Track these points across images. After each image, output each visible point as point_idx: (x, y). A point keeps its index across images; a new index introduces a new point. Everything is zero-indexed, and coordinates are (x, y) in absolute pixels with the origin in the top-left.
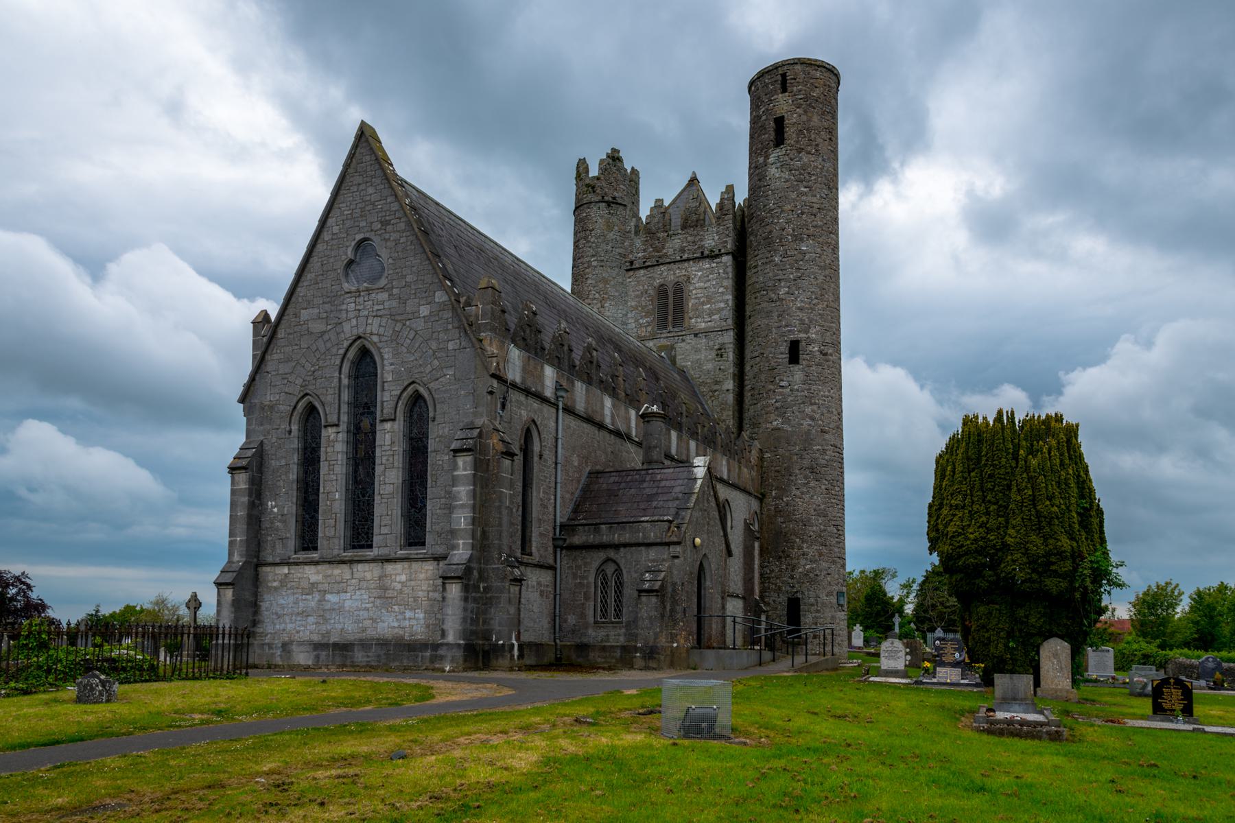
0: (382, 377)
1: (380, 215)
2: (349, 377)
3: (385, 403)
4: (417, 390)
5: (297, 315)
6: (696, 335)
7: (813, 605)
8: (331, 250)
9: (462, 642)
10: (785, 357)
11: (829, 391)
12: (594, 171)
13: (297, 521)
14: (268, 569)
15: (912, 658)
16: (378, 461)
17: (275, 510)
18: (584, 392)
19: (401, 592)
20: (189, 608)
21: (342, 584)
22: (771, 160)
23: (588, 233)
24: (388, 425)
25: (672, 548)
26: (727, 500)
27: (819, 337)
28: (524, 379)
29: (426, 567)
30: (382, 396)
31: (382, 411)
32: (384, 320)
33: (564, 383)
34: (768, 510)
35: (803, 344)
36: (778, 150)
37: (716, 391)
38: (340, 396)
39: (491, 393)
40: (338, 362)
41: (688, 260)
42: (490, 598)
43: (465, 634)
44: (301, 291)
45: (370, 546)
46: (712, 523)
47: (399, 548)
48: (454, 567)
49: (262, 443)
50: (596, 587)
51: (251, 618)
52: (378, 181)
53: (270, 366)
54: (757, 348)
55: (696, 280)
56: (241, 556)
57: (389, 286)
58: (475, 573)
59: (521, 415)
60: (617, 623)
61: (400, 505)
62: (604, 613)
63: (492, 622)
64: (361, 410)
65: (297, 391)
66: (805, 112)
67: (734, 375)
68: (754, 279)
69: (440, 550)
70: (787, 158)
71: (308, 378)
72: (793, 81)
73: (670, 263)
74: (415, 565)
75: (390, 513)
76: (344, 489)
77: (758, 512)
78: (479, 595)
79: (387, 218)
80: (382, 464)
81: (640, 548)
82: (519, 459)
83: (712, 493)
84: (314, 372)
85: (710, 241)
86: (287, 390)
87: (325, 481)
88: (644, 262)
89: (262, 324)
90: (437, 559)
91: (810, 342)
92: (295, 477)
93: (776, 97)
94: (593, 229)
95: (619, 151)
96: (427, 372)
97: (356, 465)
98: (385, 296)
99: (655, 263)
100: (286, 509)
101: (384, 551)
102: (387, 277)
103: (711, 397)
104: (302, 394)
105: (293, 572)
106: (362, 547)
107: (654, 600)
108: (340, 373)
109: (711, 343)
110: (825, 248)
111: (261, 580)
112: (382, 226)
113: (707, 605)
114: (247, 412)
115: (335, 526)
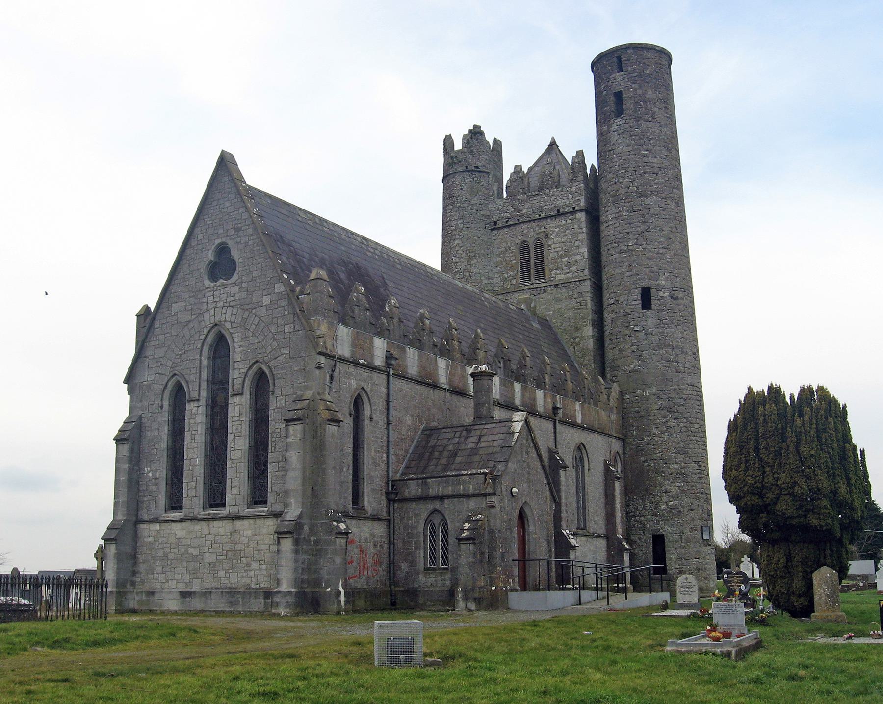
0: (233, 358)
1: (234, 223)
2: (208, 358)
3: (235, 380)
4: (261, 368)
5: (169, 308)
6: (556, 286)
7: (676, 542)
8: (196, 253)
9: (293, 590)
11: (682, 333)
12: (458, 145)
13: (166, 484)
16: (229, 431)
18: (416, 358)
19: (248, 545)
20: (97, 558)
22: (614, 127)
23: (454, 199)
24: (237, 399)
25: (488, 499)
26: (582, 443)
27: (669, 283)
28: (353, 353)
29: (268, 524)
30: (233, 374)
31: (233, 386)
32: (235, 310)
33: (395, 353)
34: (631, 449)
35: (653, 291)
36: (618, 120)
37: (577, 337)
38: (200, 376)
39: (319, 368)
40: (199, 346)
41: (546, 218)
42: (321, 550)
43: (298, 582)
44: (173, 288)
45: (224, 505)
46: (532, 472)
47: (246, 507)
48: (287, 523)
49: (141, 417)
50: (425, 536)
51: (131, 569)
52: (233, 196)
53: (149, 352)
54: (612, 295)
56: (124, 515)
57: (240, 280)
58: (306, 528)
59: (350, 384)
60: (444, 569)
61: (246, 468)
62: (434, 559)
63: (321, 571)
64: (217, 387)
65: (168, 372)
66: (640, 87)
67: (593, 322)
68: (606, 233)
69: (278, 508)
70: (627, 126)
71: (177, 361)
72: (627, 62)
73: (530, 221)
74: (259, 522)
75: (238, 475)
76: (203, 455)
77: (620, 452)
78: (310, 547)
79: (239, 225)
80: (232, 433)
81: (461, 499)
82: (348, 423)
83: (532, 445)
84: (181, 355)
85: (562, 200)
86: (160, 372)
87: (188, 448)
88: (507, 222)
89: (143, 317)
90: (277, 515)
91: (660, 288)
92: (165, 445)
93: (613, 75)
94: (459, 196)
95: (480, 127)
96: (268, 352)
97: (212, 434)
98: (236, 289)
99: (517, 222)
100: (158, 474)
101: (234, 510)
102: (238, 274)
103: (572, 343)
104: (171, 374)
105: (163, 528)
106: (217, 506)
107: (471, 547)
108: (201, 356)
109: (570, 293)
110: (669, 202)
111: (139, 536)
112: (235, 232)
113: (532, 549)
114: (131, 391)
115: (196, 488)
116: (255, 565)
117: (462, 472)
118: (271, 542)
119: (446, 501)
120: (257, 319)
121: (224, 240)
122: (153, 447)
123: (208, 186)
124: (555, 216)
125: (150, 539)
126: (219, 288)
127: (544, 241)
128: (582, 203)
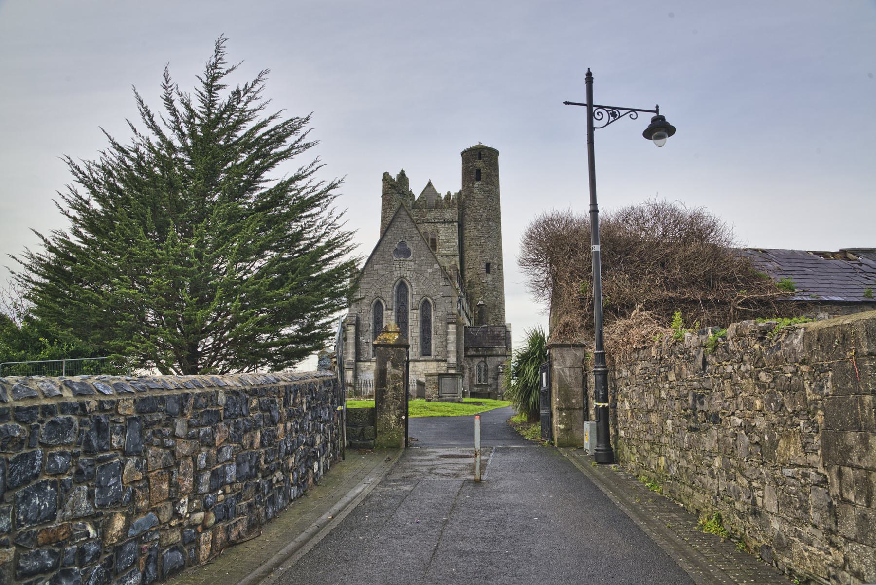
5: (372, 267)
14: (361, 363)
24: (415, 311)
32: (412, 273)
44: (374, 258)
85: (448, 215)
91: (494, 264)
98: (412, 263)
127: (436, 234)
128: (457, 219)
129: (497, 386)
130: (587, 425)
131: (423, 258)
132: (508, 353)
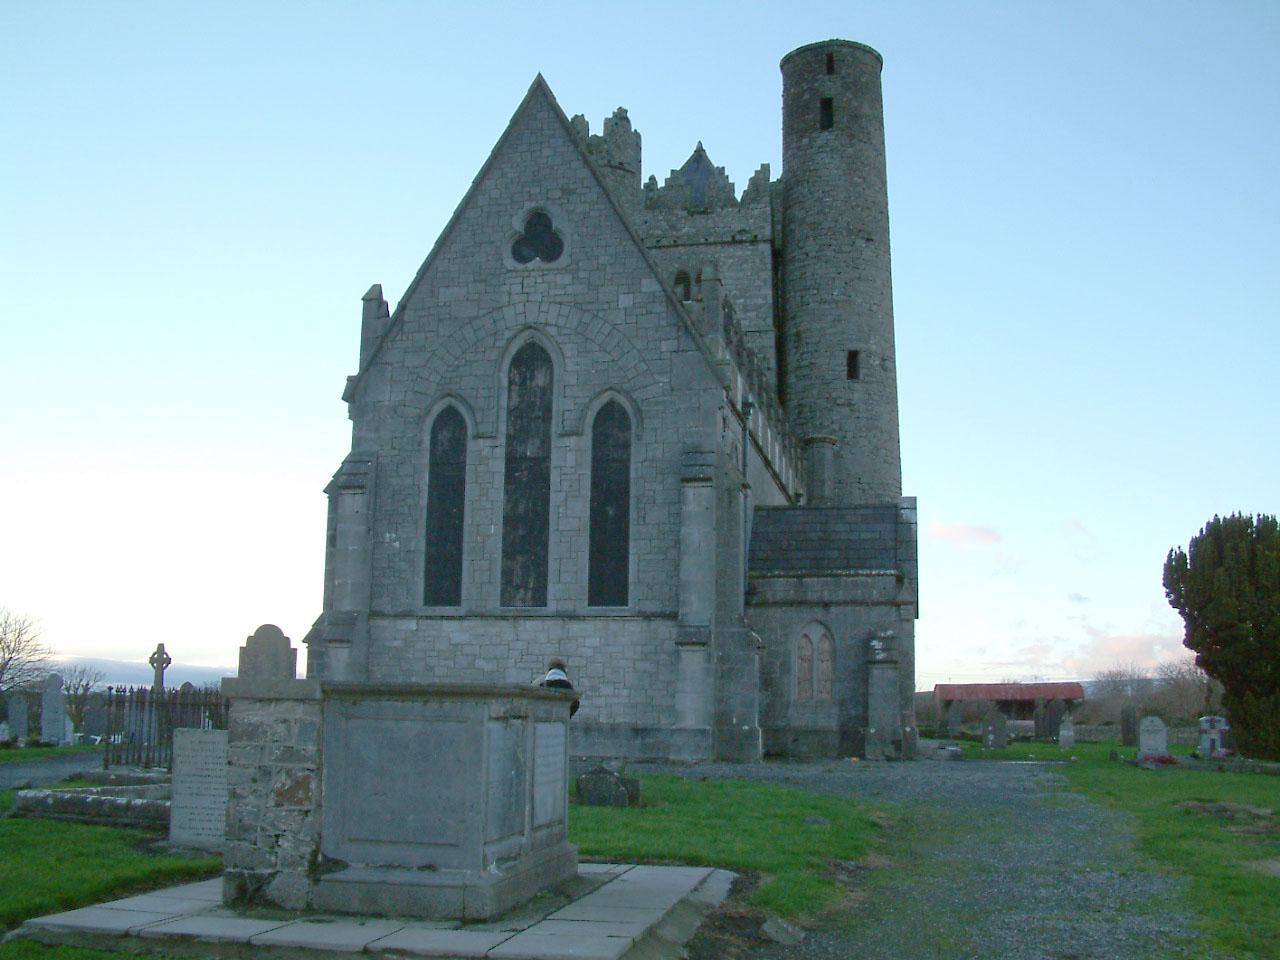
3: (567, 413)
9: (708, 728)
10: (843, 370)
14: (385, 623)
15: (996, 738)
17: (397, 544)
21: (502, 647)
24: (572, 441)
32: (565, 310)
35: (862, 356)
41: (715, 243)
55: (726, 267)
88: (658, 241)
91: (870, 354)
95: (626, 111)
98: (568, 279)
101: (568, 606)
114: (355, 414)
116: (606, 690)
117: (860, 572)
118: (636, 657)
119: (833, 609)
120: (607, 328)
121: (541, 203)
122: (402, 503)
123: (515, 121)
124: (729, 243)
125: (397, 643)
126: (533, 274)
129: (866, 707)
130: (520, 212)
131: (603, 260)
132: (904, 596)
